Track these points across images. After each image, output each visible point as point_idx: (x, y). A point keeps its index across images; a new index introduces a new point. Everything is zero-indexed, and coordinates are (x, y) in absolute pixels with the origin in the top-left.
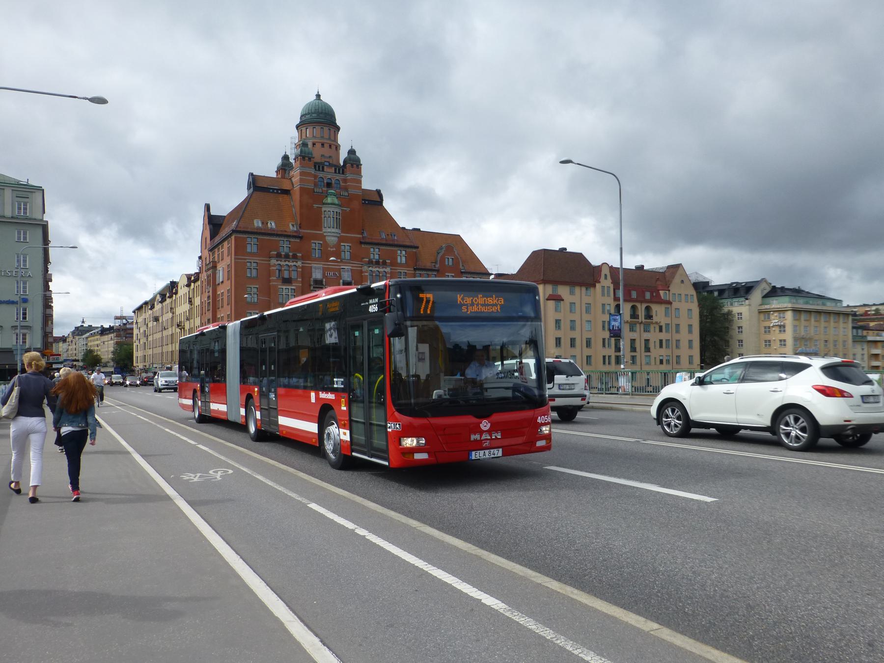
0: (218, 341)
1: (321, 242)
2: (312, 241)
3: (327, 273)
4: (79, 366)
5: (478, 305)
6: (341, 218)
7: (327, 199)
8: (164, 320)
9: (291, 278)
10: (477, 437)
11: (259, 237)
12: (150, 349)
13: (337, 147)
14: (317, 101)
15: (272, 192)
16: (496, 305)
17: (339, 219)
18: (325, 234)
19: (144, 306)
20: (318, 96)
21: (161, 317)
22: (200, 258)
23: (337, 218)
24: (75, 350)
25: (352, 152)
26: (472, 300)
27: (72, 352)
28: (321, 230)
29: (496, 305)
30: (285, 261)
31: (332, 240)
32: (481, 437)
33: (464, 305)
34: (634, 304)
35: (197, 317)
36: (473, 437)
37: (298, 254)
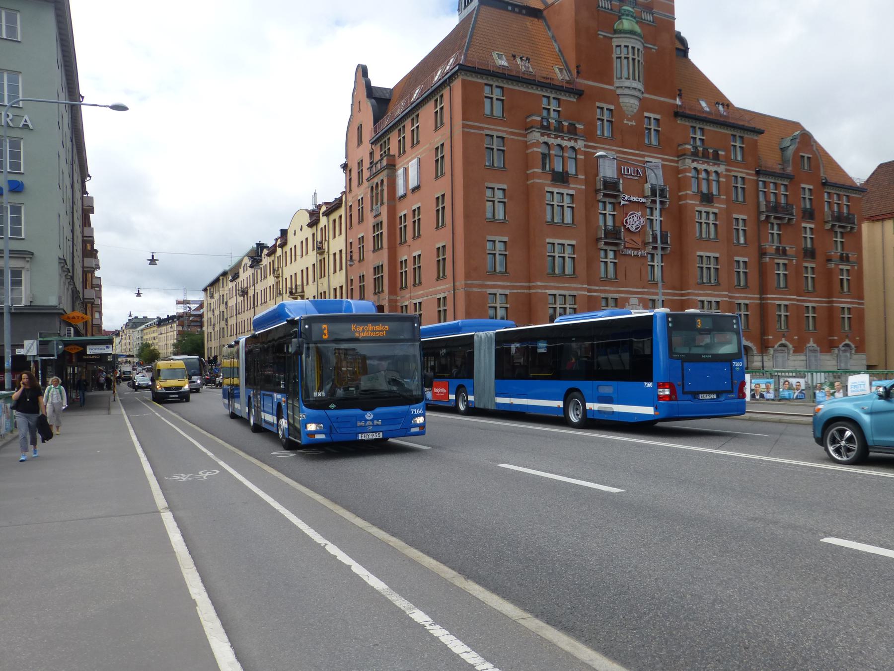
1: (612, 107)
2: (598, 104)
3: (624, 169)
4: (134, 362)
5: (368, 331)
6: (641, 61)
7: (622, 22)
9: (567, 172)
10: (362, 423)
11: (506, 86)
12: (231, 336)
15: (510, 11)
16: (383, 331)
17: (639, 61)
18: (619, 91)
19: (221, 278)
21: (252, 288)
22: (345, 167)
23: (634, 59)
24: (130, 344)
26: (363, 329)
27: (125, 347)
28: (611, 84)
29: (383, 331)
30: (556, 137)
31: (630, 104)
32: (365, 423)
33: (357, 332)
35: (335, 271)
36: (359, 424)
37: (578, 126)
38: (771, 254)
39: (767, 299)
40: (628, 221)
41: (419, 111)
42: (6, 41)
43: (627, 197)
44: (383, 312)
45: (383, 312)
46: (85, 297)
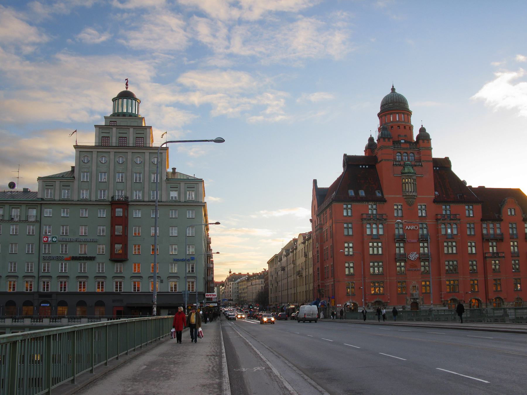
8: (289, 269)
12: (279, 292)
13: (411, 128)
14: (392, 93)
20: (393, 89)
24: (230, 288)
25: (422, 130)
40: (410, 257)
41: (327, 210)
46: (208, 279)
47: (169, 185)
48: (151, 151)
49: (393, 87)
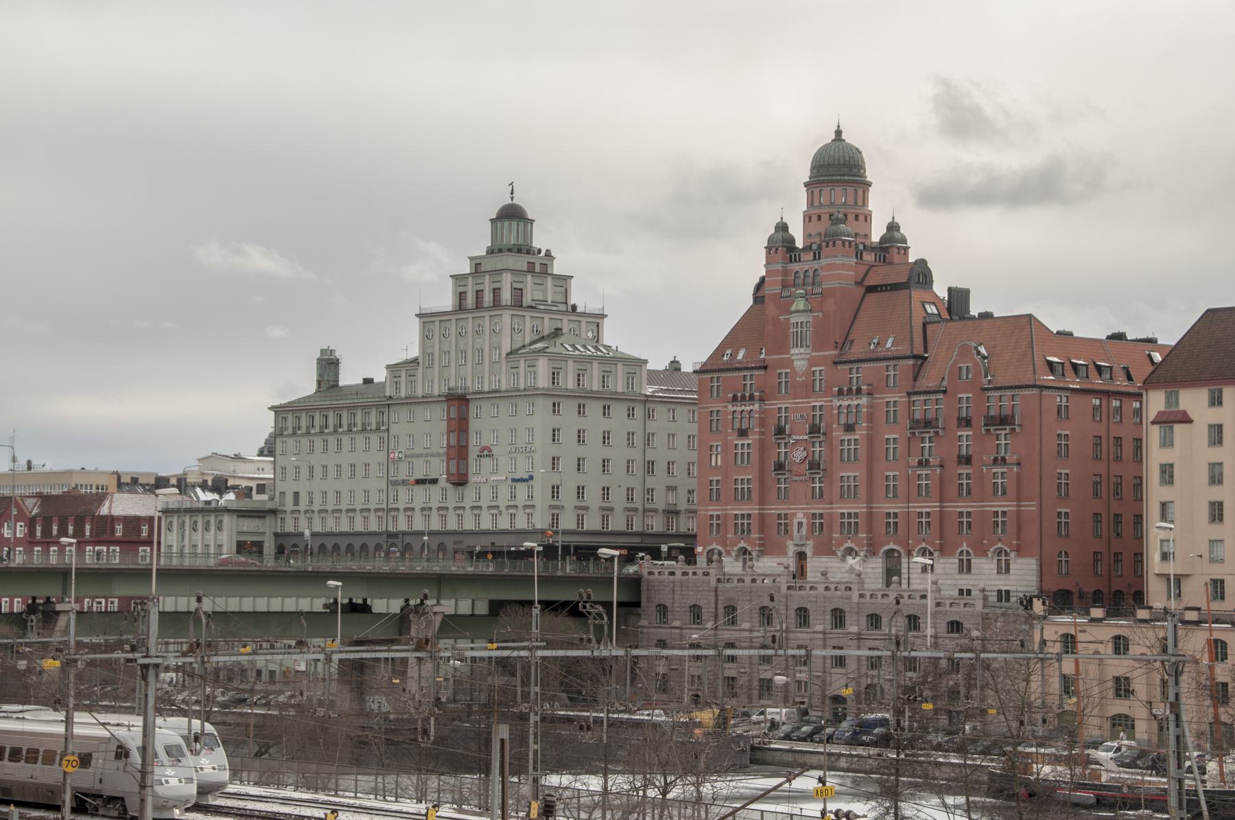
0: (693, 518)
13: (867, 218)
18: (793, 358)
20: (838, 133)
25: (893, 227)
28: (788, 353)
34: (29, 472)
38: (913, 467)
39: (867, 508)
42: (844, 337)
43: (795, 437)
44: (257, 493)
45: (257, 493)
47: (510, 365)
48: (442, 318)
49: (839, 126)
